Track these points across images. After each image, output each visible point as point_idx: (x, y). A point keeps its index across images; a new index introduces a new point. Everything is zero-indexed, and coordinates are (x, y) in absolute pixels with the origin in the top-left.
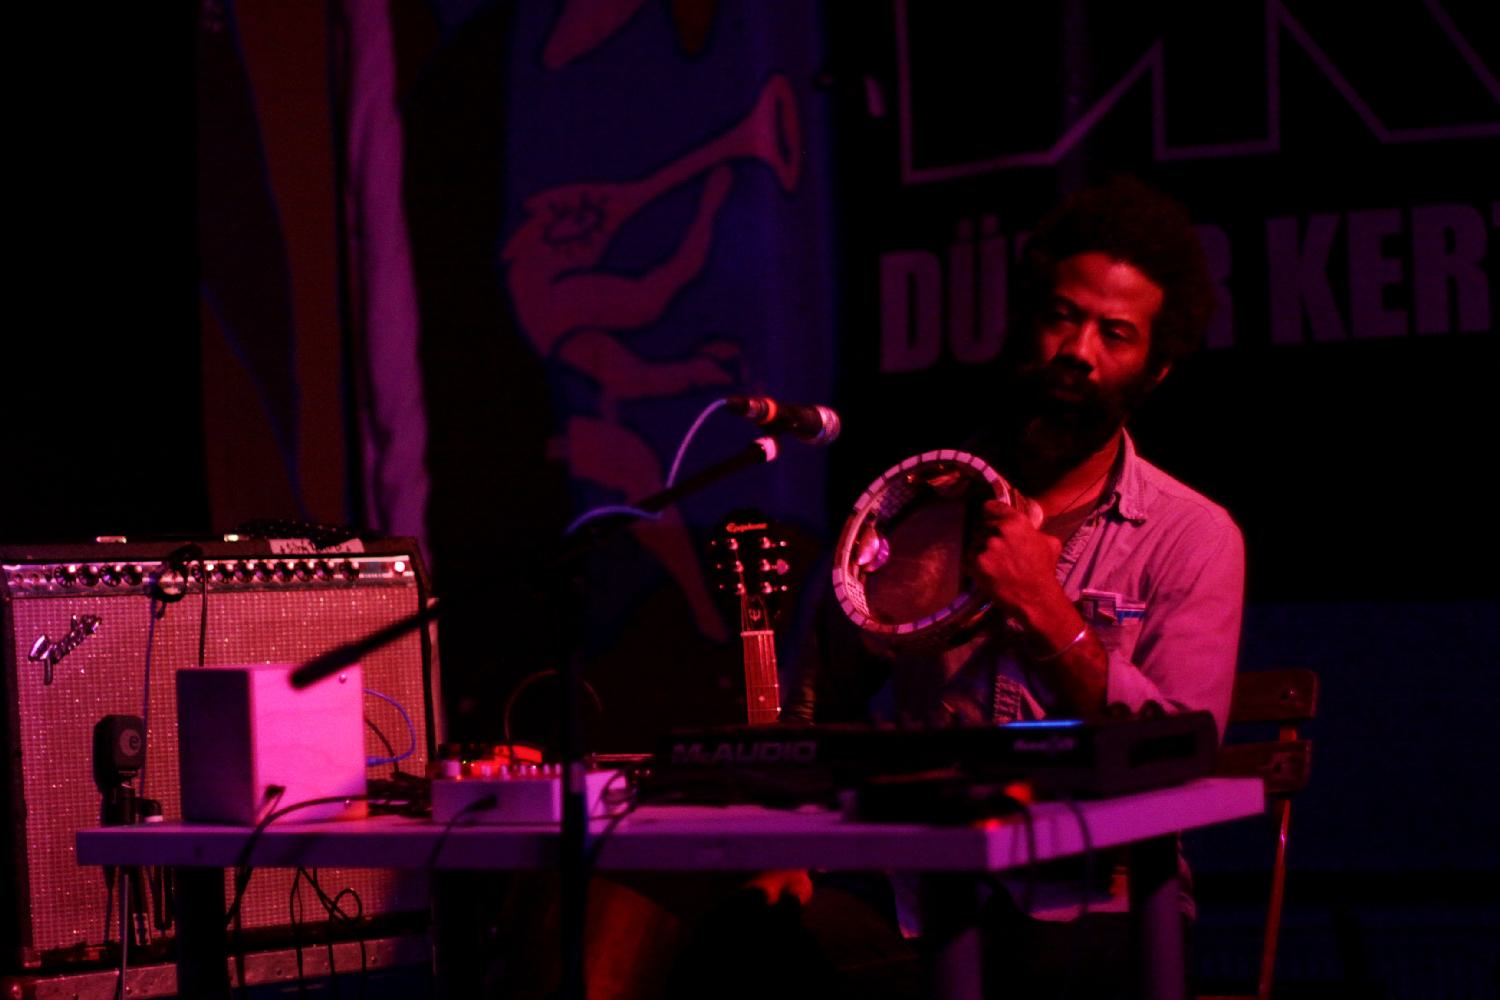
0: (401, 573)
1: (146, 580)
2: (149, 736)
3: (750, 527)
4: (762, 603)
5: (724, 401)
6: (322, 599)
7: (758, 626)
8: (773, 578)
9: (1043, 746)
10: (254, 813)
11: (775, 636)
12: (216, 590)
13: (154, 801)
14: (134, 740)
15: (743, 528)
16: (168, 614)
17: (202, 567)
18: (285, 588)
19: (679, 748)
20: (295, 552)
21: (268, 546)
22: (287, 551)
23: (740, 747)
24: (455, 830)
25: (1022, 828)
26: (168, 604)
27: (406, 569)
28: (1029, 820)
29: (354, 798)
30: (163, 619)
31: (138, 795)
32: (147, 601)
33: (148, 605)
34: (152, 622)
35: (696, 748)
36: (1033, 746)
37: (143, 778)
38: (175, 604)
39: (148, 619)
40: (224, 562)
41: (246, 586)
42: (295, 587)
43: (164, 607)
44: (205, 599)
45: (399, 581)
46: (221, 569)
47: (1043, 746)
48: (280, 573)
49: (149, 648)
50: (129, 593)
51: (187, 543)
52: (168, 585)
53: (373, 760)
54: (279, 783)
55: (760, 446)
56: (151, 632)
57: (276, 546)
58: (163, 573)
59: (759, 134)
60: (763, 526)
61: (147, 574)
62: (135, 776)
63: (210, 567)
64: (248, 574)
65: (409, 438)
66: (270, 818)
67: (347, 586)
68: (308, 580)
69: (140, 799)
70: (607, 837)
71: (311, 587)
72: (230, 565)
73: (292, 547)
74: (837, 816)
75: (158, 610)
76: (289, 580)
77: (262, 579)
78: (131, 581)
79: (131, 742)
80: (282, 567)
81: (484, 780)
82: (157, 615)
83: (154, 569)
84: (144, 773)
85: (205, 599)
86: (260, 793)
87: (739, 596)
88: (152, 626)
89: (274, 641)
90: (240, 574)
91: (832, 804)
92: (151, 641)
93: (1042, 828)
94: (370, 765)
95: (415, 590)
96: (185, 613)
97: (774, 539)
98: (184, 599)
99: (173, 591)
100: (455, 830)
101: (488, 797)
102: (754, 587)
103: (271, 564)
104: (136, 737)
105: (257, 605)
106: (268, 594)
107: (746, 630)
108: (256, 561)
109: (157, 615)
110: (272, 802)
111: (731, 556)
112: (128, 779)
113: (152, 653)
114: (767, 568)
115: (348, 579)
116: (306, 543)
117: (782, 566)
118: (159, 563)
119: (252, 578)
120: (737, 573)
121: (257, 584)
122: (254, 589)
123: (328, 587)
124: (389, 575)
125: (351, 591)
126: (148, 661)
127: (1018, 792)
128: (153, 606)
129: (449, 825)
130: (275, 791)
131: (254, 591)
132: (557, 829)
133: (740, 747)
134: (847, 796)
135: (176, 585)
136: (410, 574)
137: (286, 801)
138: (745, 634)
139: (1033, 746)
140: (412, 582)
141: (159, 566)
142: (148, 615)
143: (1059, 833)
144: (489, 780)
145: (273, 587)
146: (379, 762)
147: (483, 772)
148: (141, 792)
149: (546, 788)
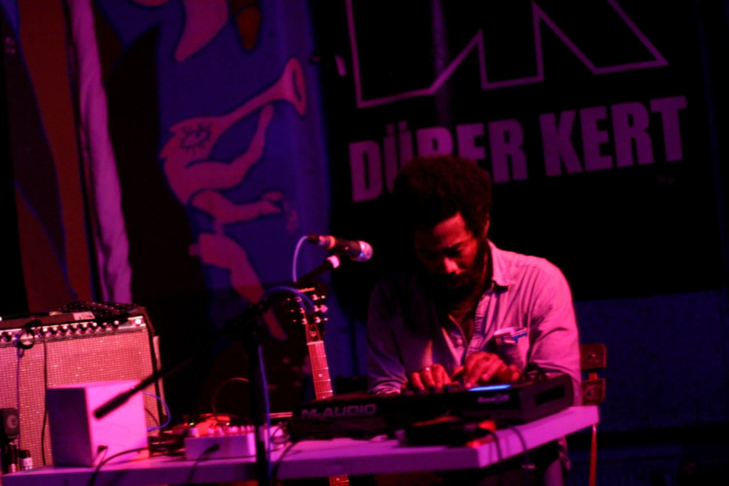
0: (139, 325)
1: (14, 339)
2: (20, 417)
3: (306, 290)
4: (316, 327)
5: (305, 238)
6: (102, 341)
7: (315, 339)
8: (319, 314)
9: (493, 399)
10: (93, 461)
11: (324, 343)
12: (49, 341)
13: (26, 451)
14: (14, 420)
15: (303, 291)
16: (26, 355)
17: (41, 330)
18: (83, 337)
19: (305, 412)
20: (86, 319)
21: (73, 317)
22: (82, 319)
23: (337, 409)
24: (201, 464)
25: (493, 445)
26: (26, 350)
27: (142, 323)
28: (496, 440)
29: (138, 450)
30: (23, 358)
31: (18, 448)
32: (15, 349)
33: (16, 351)
34: (19, 360)
35: (314, 411)
36: (488, 400)
37: (19, 439)
38: (29, 350)
39: (17, 358)
40: (52, 326)
41: (64, 338)
42: (88, 336)
43: (23, 352)
44: (45, 346)
45: (139, 330)
46: (50, 330)
47: (493, 399)
48: (80, 330)
49: (18, 373)
50: (6, 346)
51: (33, 319)
52: (25, 340)
53: (150, 428)
54: (104, 444)
55: (329, 262)
56: (18, 365)
57: (77, 316)
58: (22, 334)
59: (286, 87)
60: (312, 289)
61: (14, 336)
62: (16, 438)
63: (45, 329)
64: (64, 331)
65: (120, 249)
66: (103, 463)
67: (113, 334)
68: (93, 332)
69: (19, 450)
70: (279, 463)
71: (95, 336)
72: (55, 328)
73: (84, 316)
74: (394, 443)
75: (20, 353)
76: (85, 333)
77: (71, 333)
78: (6, 340)
79: (13, 422)
80: (80, 326)
81: (210, 436)
82: (20, 356)
83: (17, 333)
84: (20, 436)
85: (45, 346)
86: (95, 450)
87: (304, 325)
88: (18, 362)
89: (79, 364)
90: (60, 332)
91: (391, 437)
92: (18, 369)
93: (502, 442)
94: (149, 431)
95: (147, 333)
96: (36, 353)
97: (319, 295)
98: (33, 347)
99: (27, 343)
100: (201, 464)
101: (213, 446)
102: (311, 320)
103: (75, 325)
104: (14, 419)
105: (70, 347)
106: (74, 341)
107: (309, 342)
108: (67, 325)
109: (20, 356)
110: (102, 454)
111: (298, 306)
112: (13, 440)
113: (19, 376)
114: (317, 310)
115: (113, 330)
116: (91, 314)
117: (324, 309)
118: (20, 330)
119: (65, 334)
120: (302, 314)
121: (69, 336)
122: (67, 339)
123: (104, 335)
124: (133, 326)
125: (115, 336)
126: (17, 379)
127: (486, 425)
128: (18, 352)
129: (198, 460)
130: (102, 448)
131: (68, 340)
132: (254, 460)
133: (337, 409)
134: (400, 433)
135: (29, 340)
136: (144, 325)
137: (110, 453)
138: (309, 344)
139: (488, 400)
140: (144, 329)
141: (20, 331)
142: (16, 356)
143: (512, 444)
144: (213, 436)
145: (77, 337)
146: (153, 429)
147: (210, 432)
148: (19, 446)
149: (244, 440)
